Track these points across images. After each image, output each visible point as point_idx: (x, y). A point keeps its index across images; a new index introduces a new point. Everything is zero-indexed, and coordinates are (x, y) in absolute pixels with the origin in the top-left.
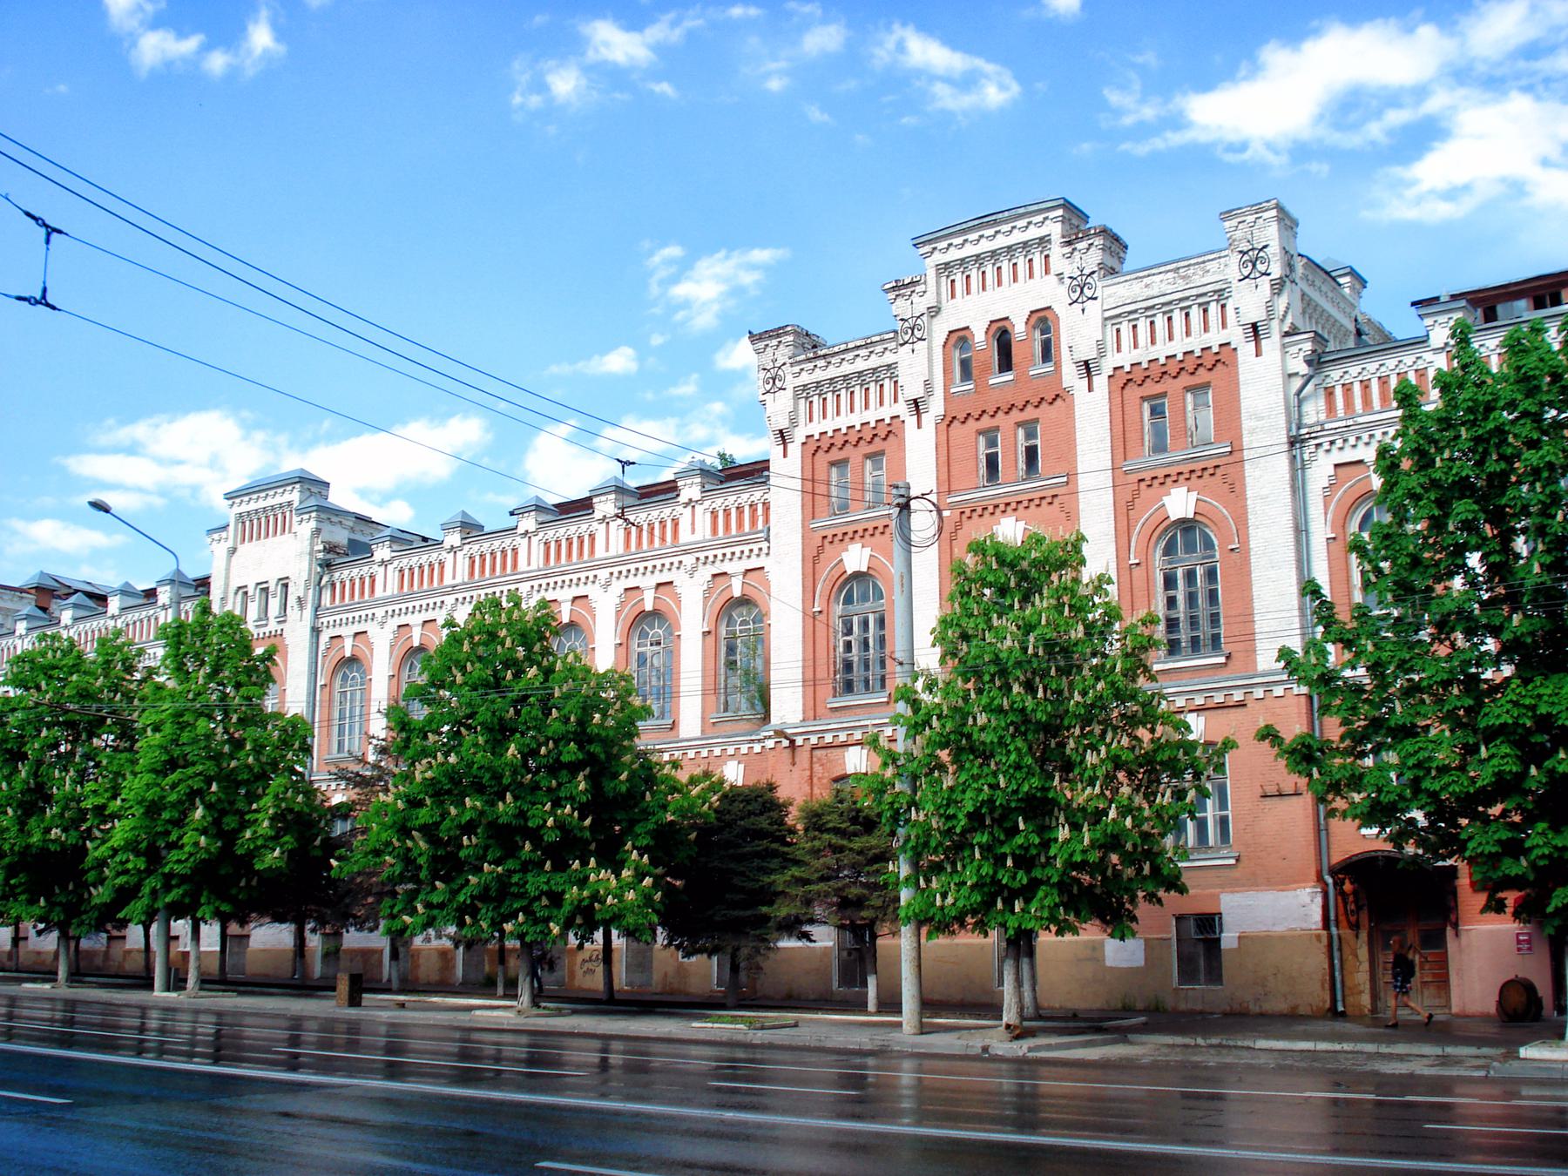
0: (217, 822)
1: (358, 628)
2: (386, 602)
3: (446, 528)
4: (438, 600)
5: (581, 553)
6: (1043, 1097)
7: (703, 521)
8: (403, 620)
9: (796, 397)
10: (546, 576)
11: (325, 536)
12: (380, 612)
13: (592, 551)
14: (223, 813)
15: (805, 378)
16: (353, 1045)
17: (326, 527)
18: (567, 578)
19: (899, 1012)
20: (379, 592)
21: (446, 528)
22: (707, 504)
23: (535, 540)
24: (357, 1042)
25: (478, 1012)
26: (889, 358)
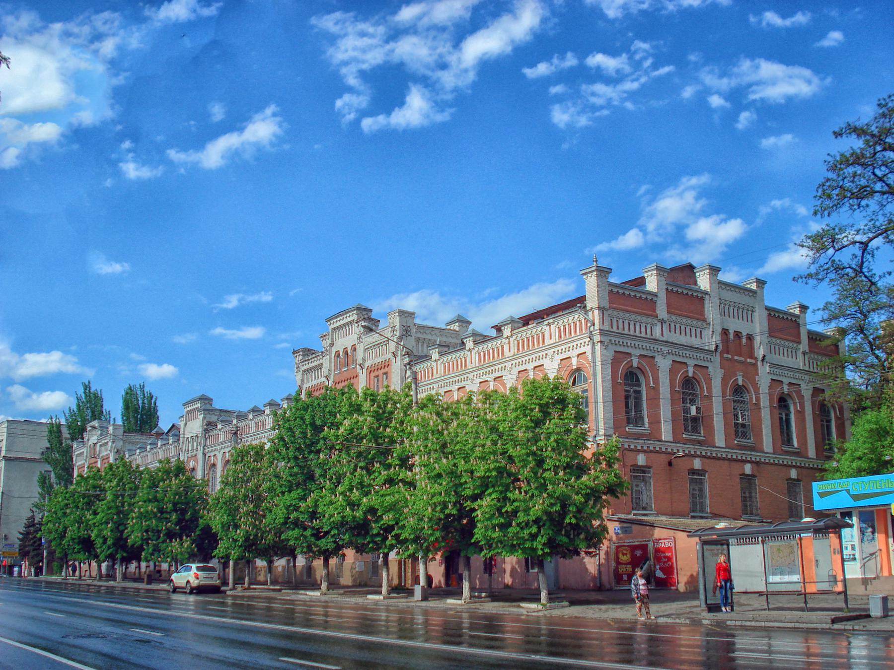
0: (117, 528)
1: (497, 375)
2: (551, 346)
3: (282, 400)
4: (544, 353)
5: (575, 332)
6: (175, 604)
7: (475, 358)
8: (522, 368)
9: (303, 374)
10: (479, 370)
11: (208, 419)
12: (508, 365)
13: (543, 342)
14: (120, 525)
15: (305, 368)
16: (187, 605)
17: (208, 416)
18: (575, 344)
19: (47, 574)
20: (547, 341)
21: (282, 400)
22: (476, 350)
23: (473, 352)
24: (309, 620)
25: (830, 652)
26: (321, 361)
